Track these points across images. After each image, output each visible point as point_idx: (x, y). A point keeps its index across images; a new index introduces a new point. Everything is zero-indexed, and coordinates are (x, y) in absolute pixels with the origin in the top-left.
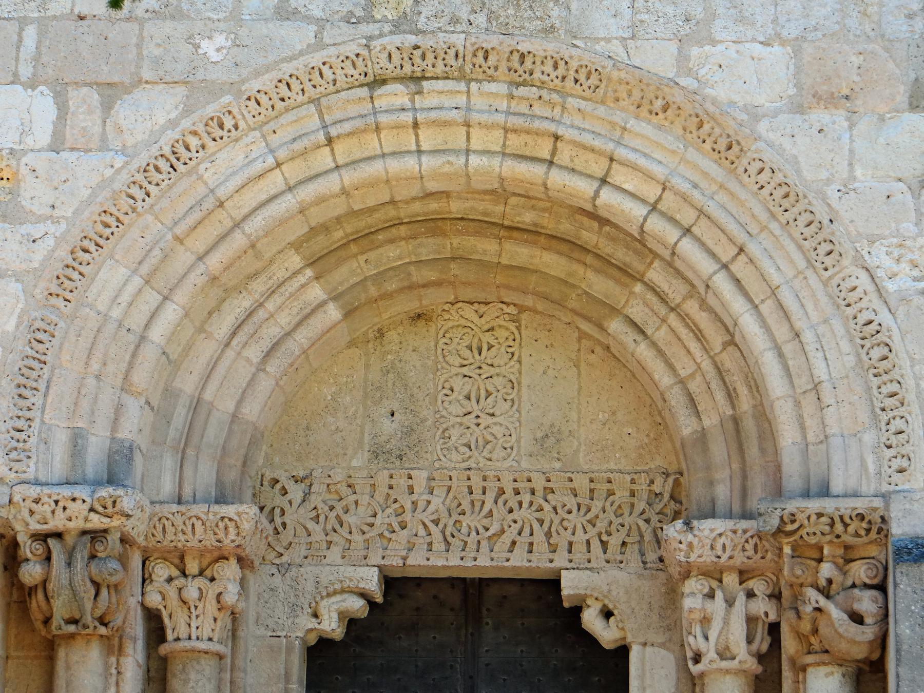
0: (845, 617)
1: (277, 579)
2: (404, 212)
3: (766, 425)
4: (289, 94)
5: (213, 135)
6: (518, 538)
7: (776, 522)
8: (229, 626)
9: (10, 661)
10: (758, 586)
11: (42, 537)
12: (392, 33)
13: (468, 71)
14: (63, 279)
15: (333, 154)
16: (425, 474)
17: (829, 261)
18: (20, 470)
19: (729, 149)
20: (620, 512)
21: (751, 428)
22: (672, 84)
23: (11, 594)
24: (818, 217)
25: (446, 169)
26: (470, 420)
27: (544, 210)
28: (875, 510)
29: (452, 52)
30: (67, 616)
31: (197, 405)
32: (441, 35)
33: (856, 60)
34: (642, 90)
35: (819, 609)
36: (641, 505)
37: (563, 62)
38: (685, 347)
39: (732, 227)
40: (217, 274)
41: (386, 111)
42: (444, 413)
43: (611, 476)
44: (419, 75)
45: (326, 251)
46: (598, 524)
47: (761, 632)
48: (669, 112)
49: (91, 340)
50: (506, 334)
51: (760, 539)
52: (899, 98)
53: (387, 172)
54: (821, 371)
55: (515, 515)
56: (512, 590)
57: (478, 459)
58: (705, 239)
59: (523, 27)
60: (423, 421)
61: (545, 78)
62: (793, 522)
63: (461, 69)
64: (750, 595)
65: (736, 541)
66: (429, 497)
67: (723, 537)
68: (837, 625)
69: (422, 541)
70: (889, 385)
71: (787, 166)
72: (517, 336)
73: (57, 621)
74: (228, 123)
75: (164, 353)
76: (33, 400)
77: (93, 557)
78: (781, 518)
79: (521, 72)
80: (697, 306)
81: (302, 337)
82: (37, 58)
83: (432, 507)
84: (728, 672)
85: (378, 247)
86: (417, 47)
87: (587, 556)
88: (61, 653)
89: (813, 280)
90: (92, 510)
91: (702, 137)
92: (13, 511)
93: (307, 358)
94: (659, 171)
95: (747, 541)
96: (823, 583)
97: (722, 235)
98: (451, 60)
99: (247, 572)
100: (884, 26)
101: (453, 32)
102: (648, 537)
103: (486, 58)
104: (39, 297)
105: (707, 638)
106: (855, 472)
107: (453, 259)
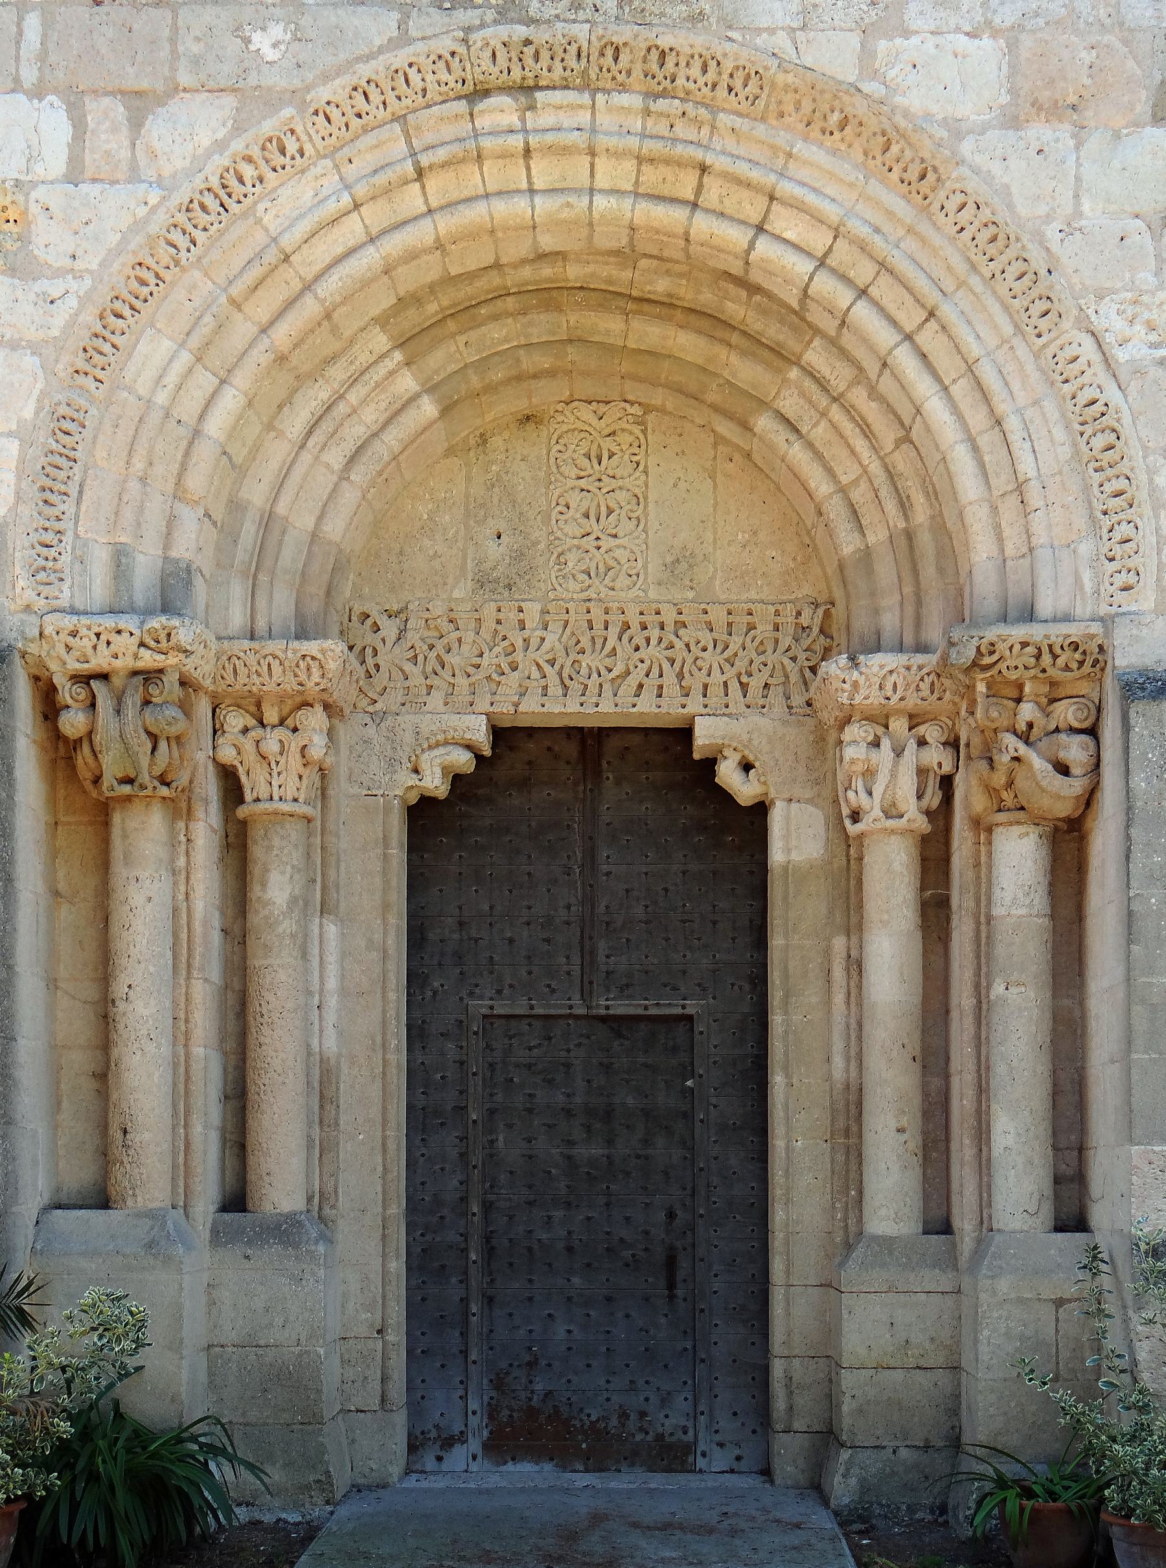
0: (1050, 767)
1: (371, 731)
2: (512, 279)
3: (946, 540)
4: (367, 108)
5: (273, 164)
6: (645, 681)
7: (972, 653)
8: (318, 784)
9: (60, 828)
10: (931, 732)
11: (84, 679)
12: (496, 22)
13: (593, 76)
14: (91, 352)
15: (424, 194)
16: (538, 607)
17: (1044, 324)
18: (51, 595)
19: (922, 179)
20: (761, 649)
21: (929, 547)
22: (852, 90)
23: (57, 749)
24: (1034, 265)
25: (565, 214)
26: (589, 543)
27: (681, 275)
28: (1092, 637)
29: (573, 49)
30: (120, 775)
31: (268, 521)
32: (559, 25)
33: (1087, 57)
34: (814, 100)
35: (1017, 759)
36: (786, 641)
37: (714, 63)
38: (849, 446)
39: (922, 284)
40: (286, 351)
41: (490, 134)
42: (559, 534)
43: (752, 606)
44: (531, 83)
45: (417, 329)
46: (737, 663)
47: (932, 785)
48: (848, 129)
49: (131, 433)
50: (631, 439)
51: (939, 676)
52: (1139, 108)
53: (492, 218)
54: (1027, 466)
55: (642, 654)
56: (637, 739)
57: (598, 588)
58: (884, 302)
59: (662, 14)
60: (536, 543)
61: (691, 85)
62: (992, 653)
63: (585, 73)
64: (922, 743)
65: (909, 679)
66: (544, 634)
67: (895, 675)
68: (1039, 778)
69: (535, 684)
70: (1114, 481)
71: (996, 199)
72: (643, 440)
73: (108, 780)
74: (292, 147)
75: (225, 453)
76: (62, 507)
77: (147, 702)
78: (978, 648)
79: (660, 77)
80: (865, 394)
81: (392, 438)
82: (42, 57)
83: (547, 645)
84: (893, 832)
85: (480, 325)
86: (528, 42)
87: (725, 700)
88: (116, 818)
89: (1022, 351)
90: (142, 644)
91: (888, 164)
92: (45, 647)
93: (399, 464)
94: (832, 212)
95: (922, 680)
96: (1022, 726)
97: (907, 296)
98: (572, 62)
99: (336, 721)
100: (1123, 10)
101: (574, 21)
102: (794, 677)
103: (616, 59)
104: (62, 374)
105: (870, 794)
106: (1069, 591)
107: (570, 341)
